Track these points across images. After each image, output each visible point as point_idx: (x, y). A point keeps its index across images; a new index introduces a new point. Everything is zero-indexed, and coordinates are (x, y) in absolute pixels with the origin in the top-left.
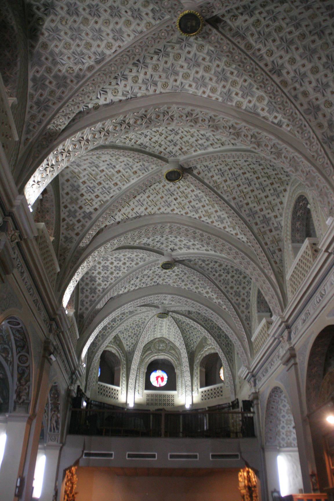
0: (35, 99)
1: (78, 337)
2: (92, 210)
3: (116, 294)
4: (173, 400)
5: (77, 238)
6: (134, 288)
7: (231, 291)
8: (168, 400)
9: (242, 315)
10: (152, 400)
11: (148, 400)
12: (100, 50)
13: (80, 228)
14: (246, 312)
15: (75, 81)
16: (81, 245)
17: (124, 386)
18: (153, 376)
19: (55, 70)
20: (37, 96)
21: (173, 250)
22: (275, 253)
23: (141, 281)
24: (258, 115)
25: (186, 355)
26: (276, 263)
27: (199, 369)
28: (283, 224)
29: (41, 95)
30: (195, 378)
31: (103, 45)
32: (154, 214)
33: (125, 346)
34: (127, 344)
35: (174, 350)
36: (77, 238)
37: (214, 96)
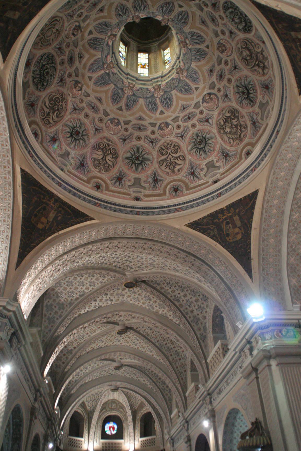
0: (47, 317)
1: (54, 392)
2: (73, 348)
3: (83, 383)
4: (121, 447)
5: (63, 365)
6: (95, 377)
7: (159, 381)
8: (117, 447)
9: (166, 397)
10: (106, 447)
11: (103, 447)
12: (82, 290)
13: (65, 359)
14: (169, 395)
15: (69, 306)
16: (66, 370)
17: (87, 437)
18: (107, 427)
19: (58, 300)
20: (48, 314)
21: (121, 359)
22: (182, 372)
23: (100, 373)
24: (168, 318)
25: (131, 414)
26: (182, 379)
27: (139, 423)
28: (187, 355)
29: (50, 314)
30: (136, 431)
31: (84, 288)
32: (110, 345)
33: (87, 406)
34: (89, 406)
35: (122, 409)
36: (63, 365)
37: (144, 306)
